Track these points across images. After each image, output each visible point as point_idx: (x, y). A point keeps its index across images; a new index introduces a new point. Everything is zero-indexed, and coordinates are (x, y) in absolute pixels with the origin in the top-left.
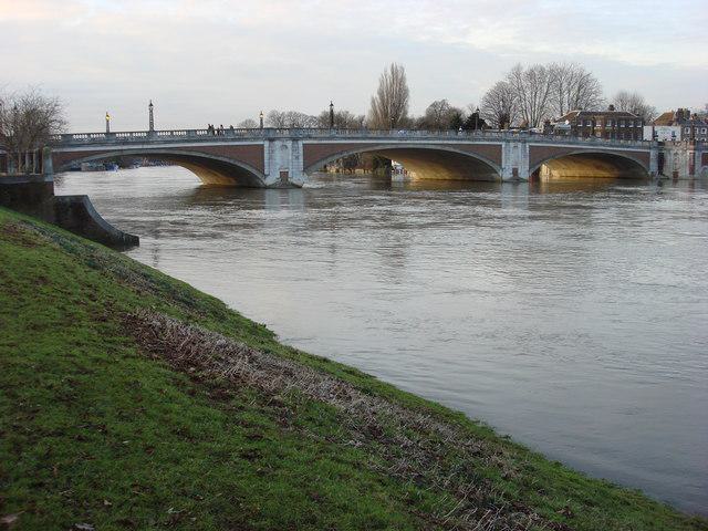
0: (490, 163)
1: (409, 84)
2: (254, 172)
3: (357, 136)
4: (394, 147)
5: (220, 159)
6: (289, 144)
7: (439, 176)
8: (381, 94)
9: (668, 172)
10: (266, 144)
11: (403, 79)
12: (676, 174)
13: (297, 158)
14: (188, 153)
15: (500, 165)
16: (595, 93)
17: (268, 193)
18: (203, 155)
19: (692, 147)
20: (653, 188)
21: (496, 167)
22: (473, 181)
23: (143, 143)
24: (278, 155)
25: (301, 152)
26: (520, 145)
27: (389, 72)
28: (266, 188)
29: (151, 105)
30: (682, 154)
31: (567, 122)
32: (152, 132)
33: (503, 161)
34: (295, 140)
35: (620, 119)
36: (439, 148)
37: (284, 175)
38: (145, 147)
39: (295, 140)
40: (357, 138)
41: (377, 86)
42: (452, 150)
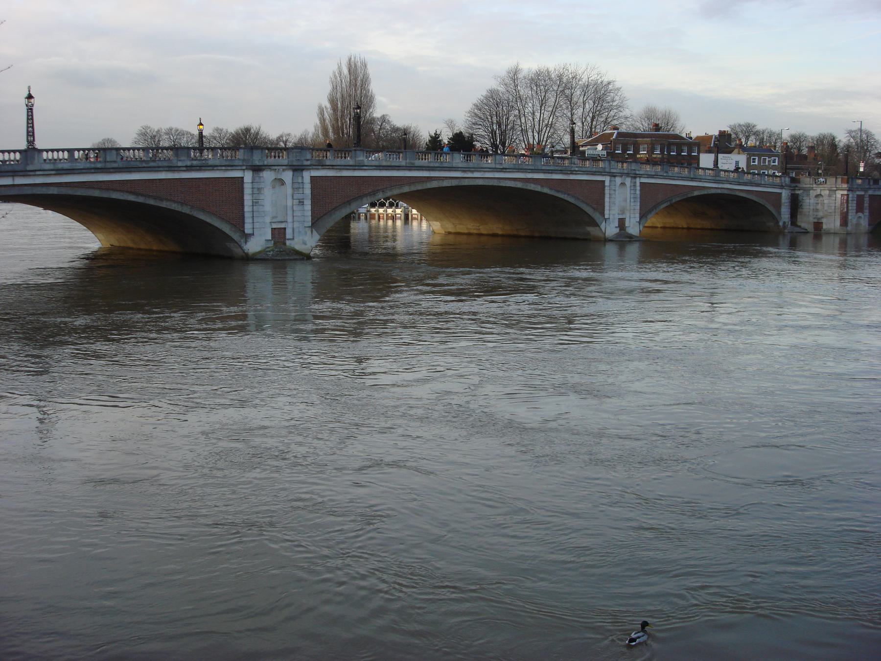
0: (588, 210)
1: (374, 87)
2: (226, 228)
3: (396, 163)
4: (454, 183)
5: (164, 204)
6: (288, 176)
7: (484, 230)
8: (333, 101)
9: (806, 222)
10: (248, 176)
11: (365, 81)
12: (818, 225)
13: (301, 203)
14: (105, 195)
15: (603, 214)
16: (619, 107)
17: (255, 271)
18: (132, 198)
19: (845, 186)
20: (783, 251)
21: (596, 216)
22: (548, 238)
23: (14, 173)
24: (268, 196)
25: (308, 191)
26: (628, 181)
27: (345, 71)
28: (248, 259)
29: (30, 97)
30: (830, 196)
31: (600, 147)
32: (31, 151)
33: (607, 208)
34: (297, 169)
35: (670, 144)
36: (519, 185)
37: (279, 234)
38: (19, 181)
39: (297, 169)
40: (398, 168)
41: (328, 88)
42: (538, 188)
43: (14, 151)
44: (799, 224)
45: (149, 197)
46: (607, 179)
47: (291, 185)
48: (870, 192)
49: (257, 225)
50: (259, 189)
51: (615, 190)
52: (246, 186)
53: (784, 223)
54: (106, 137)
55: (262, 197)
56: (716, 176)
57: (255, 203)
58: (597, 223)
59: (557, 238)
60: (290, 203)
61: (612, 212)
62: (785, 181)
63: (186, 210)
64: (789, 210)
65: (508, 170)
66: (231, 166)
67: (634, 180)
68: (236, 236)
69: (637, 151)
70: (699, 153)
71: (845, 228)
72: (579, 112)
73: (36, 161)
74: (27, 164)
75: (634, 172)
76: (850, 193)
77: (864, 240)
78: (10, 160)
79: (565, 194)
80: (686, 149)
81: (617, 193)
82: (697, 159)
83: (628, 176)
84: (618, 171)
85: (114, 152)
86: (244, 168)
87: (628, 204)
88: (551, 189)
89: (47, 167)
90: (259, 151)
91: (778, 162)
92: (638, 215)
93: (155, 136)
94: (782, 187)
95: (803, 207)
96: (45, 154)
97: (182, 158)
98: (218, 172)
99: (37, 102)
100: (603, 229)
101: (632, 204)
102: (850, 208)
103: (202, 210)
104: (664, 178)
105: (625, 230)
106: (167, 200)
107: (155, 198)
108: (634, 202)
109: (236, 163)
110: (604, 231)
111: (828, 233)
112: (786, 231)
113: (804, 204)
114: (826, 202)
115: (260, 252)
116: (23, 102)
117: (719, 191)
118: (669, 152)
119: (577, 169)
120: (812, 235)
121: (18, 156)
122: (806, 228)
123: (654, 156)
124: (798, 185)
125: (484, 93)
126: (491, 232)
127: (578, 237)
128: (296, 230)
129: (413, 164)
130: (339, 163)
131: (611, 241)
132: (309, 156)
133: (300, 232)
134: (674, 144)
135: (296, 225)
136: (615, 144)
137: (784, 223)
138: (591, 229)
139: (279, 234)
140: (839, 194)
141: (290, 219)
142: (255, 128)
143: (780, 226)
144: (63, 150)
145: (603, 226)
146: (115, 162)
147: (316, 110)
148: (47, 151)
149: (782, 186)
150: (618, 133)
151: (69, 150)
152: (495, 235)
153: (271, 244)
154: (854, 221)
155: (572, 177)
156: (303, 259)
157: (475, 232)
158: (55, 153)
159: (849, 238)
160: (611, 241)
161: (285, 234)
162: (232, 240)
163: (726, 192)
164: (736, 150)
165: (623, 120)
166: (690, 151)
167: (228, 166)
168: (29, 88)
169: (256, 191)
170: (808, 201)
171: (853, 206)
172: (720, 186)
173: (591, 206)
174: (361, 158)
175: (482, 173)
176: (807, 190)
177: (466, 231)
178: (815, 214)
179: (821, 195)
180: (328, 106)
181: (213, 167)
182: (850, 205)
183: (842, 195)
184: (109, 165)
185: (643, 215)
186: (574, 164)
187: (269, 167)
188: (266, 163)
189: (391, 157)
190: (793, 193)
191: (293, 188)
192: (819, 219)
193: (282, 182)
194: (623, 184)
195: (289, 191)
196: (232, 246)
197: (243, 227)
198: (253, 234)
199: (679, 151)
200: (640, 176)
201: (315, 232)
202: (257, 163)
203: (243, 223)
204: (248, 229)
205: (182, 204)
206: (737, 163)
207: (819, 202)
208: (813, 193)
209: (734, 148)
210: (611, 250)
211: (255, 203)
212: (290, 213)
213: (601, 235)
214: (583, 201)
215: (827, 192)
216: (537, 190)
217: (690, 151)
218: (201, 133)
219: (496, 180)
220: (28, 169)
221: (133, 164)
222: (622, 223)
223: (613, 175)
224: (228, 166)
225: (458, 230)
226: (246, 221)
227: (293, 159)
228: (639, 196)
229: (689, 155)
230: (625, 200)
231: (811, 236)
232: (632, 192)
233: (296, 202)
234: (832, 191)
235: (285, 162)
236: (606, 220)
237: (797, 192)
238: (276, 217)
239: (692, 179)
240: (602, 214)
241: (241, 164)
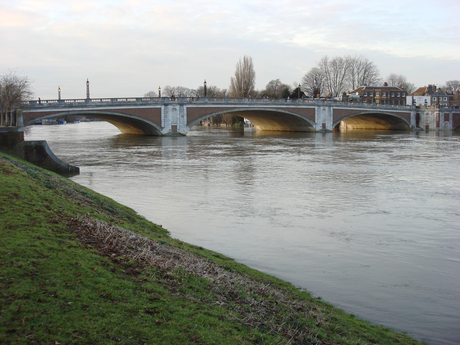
1: (256, 69)
2: (155, 125)
4: (245, 109)
5: (133, 117)
6: (178, 107)
8: (237, 75)
9: (422, 126)
10: (163, 107)
12: (427, 127)
13: (183, 116)
14: (112, 114)
19: (438, 109)
21: (311, 122)
22: (297, 131)
23: (82, 106)
26: (327, 108)
28: (163, 136)
29: (88, 82)
30: (432, 114)
31: (357, 94)
32: (88, 100)
34: (181, 105)
36: (274, 110)
37: (174, 128)
39: (181, 105)
40: (221, 104)
41: (235, 70)
42: (283, 111)
43: (72, 100)
44: (420, 126)
45: (127, 114)
46: (316, 108)
47: (179, 110)
48: (453, 112)
50: (167, 112)
51: (320, 112)
52: (162, 111)
53: (412, 126)
55: (168, 115)
57: (165, 117)
59: (299, 132)
60: (178, 116)
61: (319, 121)
62: (412, 108)
63: (140, 119)
65: (90, 106)
66: (156, 104)
68: (158, 128)
69: (375, 95)
70: (406, 96)
71: (437, 128)
73: (90, 103)
74: (87, 104)
76: (440, 112)
77: (451, 133)
78: (68, 103)
79: (296, 113)
80: (399, 94)
81: (321, 113)
82: (405, 99)
85: (116, 100)
87: (327, 118)
88: (289, 111)
90: (167, 98)
92: (332, 122)
93: (172, 90)
94: (411, 110)
97: (139, 101)
99: (90, 83)
100: (315, 128)
102: (441, 119)
103: (146, 119)
104: (345, 106)
105: (325, 128)
106: (134, 115)
107: (129, 115)
109: (159, 103)
110: (315, 128)
111: (431, 130)
112: (413, 129)
113: (422, 118)
114: (430, 116)
115: (167, 134)
116: (86, 83)
117: (375, 112)
119: (301, 104)
121: (84, 101)
123: (383, 97)
124: (419, 109)
125: (310, 70)
126: (277, 130)
129: (228, 102)
130: (197, 103)
134: (393, 92)
135: (181, 124)
136: (364, 92)
137: (412, 126)
138: (310, 127)
139: (174, 128)
140: (435, 113)
141: (178, 122)
143: (410, 127)
144: (99, 99)
145: (314, 126)
146: (116, 103)
147: (230, 80)
150: (366, 87)
151: (126, 98)
154: (443, 125)
155: (299, 107)
156: (181, 136)
157: (272, 129)
158: (82, 100)
159: (440, 132)
161: (177, 127)
162: (157, 130)
163: (379, 112)
164: (426, 94)
165: (377, 81)
168: (88, 79)
169: (165, 112)
171: (442, 118)
172: (375, 110)
176: (423, 112)
177: (269, 129)
178: (426, 122)
179: (428, 113)
180: (235, 77)
181: (150, 104)
182: (440, 118)
184: (114, 104)
185: (335, 122)
186: (300, 102)
187: (170, 104)
188: (169, 103)
189: (219, 100)
191: (180, 112)
192: (427, 124)
193: (176, 109)
194: (324, 109)
195: (178, 112)
196: (157, 131)
197: (161, 125)
199: (396, 95)
200: (333, 106)
201: (188, 127)
203: (161, 123)
205: (139, 117)
206: (426, 100)
208: (425, 113)
210: (319, 135)
211: (165, 117)
212: (178, 120)
214: (304, 116)
215: (431, 112)
217: (401, 95)
218: (205, 86)
221: (122, 104)
222: (324, 125)
223: (319, 106)
228: (332, 114)
229: (401, 97)
231: (424, 131)
233: (181, 116)
234: (433, 112)
235: (177, 102)
237: (419, 112)
239: (360, 107)
240: (314, 121)
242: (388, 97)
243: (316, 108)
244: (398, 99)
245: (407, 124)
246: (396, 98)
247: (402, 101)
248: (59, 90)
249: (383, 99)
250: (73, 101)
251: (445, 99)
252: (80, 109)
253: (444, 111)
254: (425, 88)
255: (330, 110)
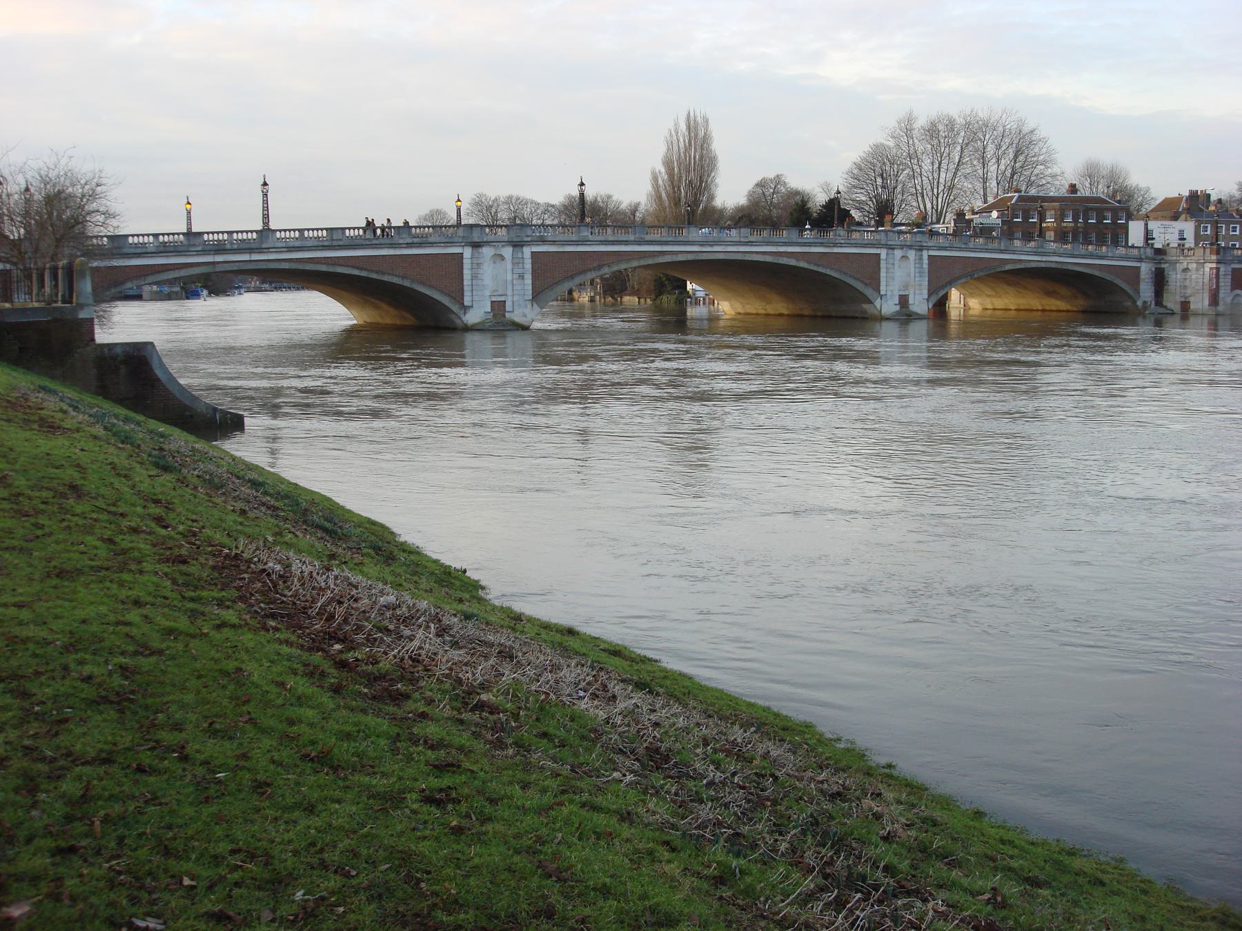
1: (719, 146)
2: (445, 301)
3: (624, 238)
4: (690, 257)
5: (386, 278)
6: (508, 252)
7: (771, 309)
8: (668, 164)
10: (467, 252)
12: (1185, 305)
13: (521, 277)
14: (331, 269)
16: (1044, 163)
17: (471, 339)
18: (356, 272)
19: (1214, 257)
21: (868, 292)
22: (830, 317)
23: (251, 250)
26: (912, 254)
28: (467, 329)
29: (265, 184)
30: (1197, 270)
31: (995, 214)
32: (266, 232)
33: (883, 283)
34: (517, 245)
36: (769, 259)
37: (498, 307)
38: (255, 257)
39: (517, 245)
40: (626, 243)
41: (661, 150)
42: (793, 262)
44: (1164, 304)
45: (372, 271)
46: (883, 253)
49: (475, 298)
51: (893, 264)
53: (1145, 302)
54: (435, 207)
55: (481, 272)
56: (1038, 248)
58: (868, 299)
59: (837, 317)
60: (509, 277)
61: (890, 288)
63: (406, 283)
64: (1153, 288)
66: (450, 243)
67: (920, 253)
68: (455, 308)
71: (1213, 308)
72: (993, 168)
74: (262, 243)
75: (920, 244)
76: (1219, 266)
80: (1109, 215)
81: (896, 267)
82: (1125, 228)
83: (911, 249)
84: (899, 243)
85: (340, 231)
86: (463, 244)
88: (809, 262)
89: (279, 245)
90: (479, 229)
91: (1240, 231)
92: (925, 292)
93: (491, 206)
94: (1140, 260)
95: (1170, 284)
96: (130, 238)
97: (404, 236)
98: (437, 248)
99: (270, 187)
100: (878, 307)
101: (917, 279)
102: (1221, 284)
103: (422, 283)
105: (908, 308)
106: (389, 274)
107: (377, 272)
108: (920, 276)
109: (456, 240)
111: (1196, 314)
112: (1147, 312)
115: (478, 324)
116: (259, 188)
117: (1043, 265)
118: (1086, 219)
119: (843, 242)
120: (1179, 316)
121: (255, 235)
122: (1173, 308)
123: (1065, 225)
124: (1164, 257)
126: (777, 312)
127: (857, 315)
128: (516, 304)
131: (888, 319)
132: (529, 233)
133: (519, 305)
134: (1092, 209)
135: (516, 298)
137: (1145, 302)
138: (865, 306)
139: (498, 307)
140: (1208, 266)
141: (509, 293)
142: (591, 197)
145: (878, 303)
148: (133, 236)
149: (1141, 258)
152: (781, 315)
153: (490, 316)
154: (1229, 300)
155: (836, 250)
160: (888, 319)
161: (505, 307)
162: (452, 312)
163: (1054, 266)
164: (1183, 216)
165: (1049, 179)
166: (1115, 218)
167: (447, 243)
168: (264, 176)
169: (475, 266)
170: (1174, 276)
172: (1044, 259)
173: (862, 282)
174: (586, 234)
175: (723, 247)
177: (754, 312)
178: (1182, 291)
180: (663, 170)
181: (432, 244)
182: (1221, 280)
183: (1211, 268)
184: (335, 243)
186: (839, 236)
187: (488, 243)
188: (485, 240)
189: (620, 232)
190: (1158, 266)
191: (513, 263)
192: (1186, 297)
193: (502, 258)
194: (904, 257)
195: (509, 266)
196: (453, 316)
197: (463, 300)
198: (472, 307)
199: (1101, 218)
200: (928, 248)
201: (535, 305)
202: (477, 240)
204: (467, 302)
205: (403, 278)
206: (1181, 232)
207: (1188, 277)
208: (1180, 267)
209: (1181, 213)
212: (510, 287)
213: (876, 312)
214: (850, 276)
216: (791, 264)
217: (1115, 218)
219: (739, 254)
220: (263, 246)
221: (357, 242)
222: (904, 300)
224: (447, 243)
225: (748, 311)
226: (465, 294)
227: (514, 235)
228: (927, 270)
229: (1114, 223)
230: (909, 275)
232: (917, 266)
233: (516, 276)
234: (1201, 265)
236: (881, 296)
237: (1163, 266)
238: (497, 291)
241: (460, 240)
242: (1079, 225)
243: (883, 253)
244: (1106, 228)
245: (1130, 297)
246: (1101, 226)
247: (1118, 235)
248: (188, 206)
249: (1065, 230)
250: (226, 236)
251: (1234, 229)
252: (246, 257)
253: (1232, 262)
254: (1179, 199)
255: (921, 259)
